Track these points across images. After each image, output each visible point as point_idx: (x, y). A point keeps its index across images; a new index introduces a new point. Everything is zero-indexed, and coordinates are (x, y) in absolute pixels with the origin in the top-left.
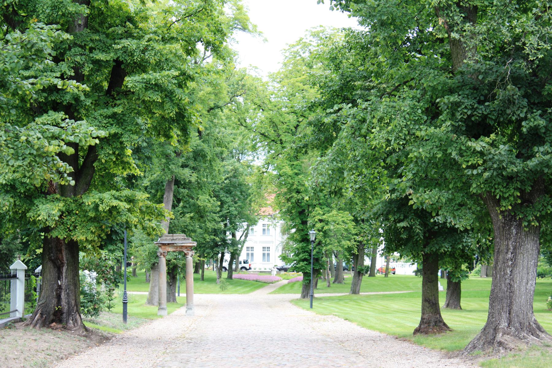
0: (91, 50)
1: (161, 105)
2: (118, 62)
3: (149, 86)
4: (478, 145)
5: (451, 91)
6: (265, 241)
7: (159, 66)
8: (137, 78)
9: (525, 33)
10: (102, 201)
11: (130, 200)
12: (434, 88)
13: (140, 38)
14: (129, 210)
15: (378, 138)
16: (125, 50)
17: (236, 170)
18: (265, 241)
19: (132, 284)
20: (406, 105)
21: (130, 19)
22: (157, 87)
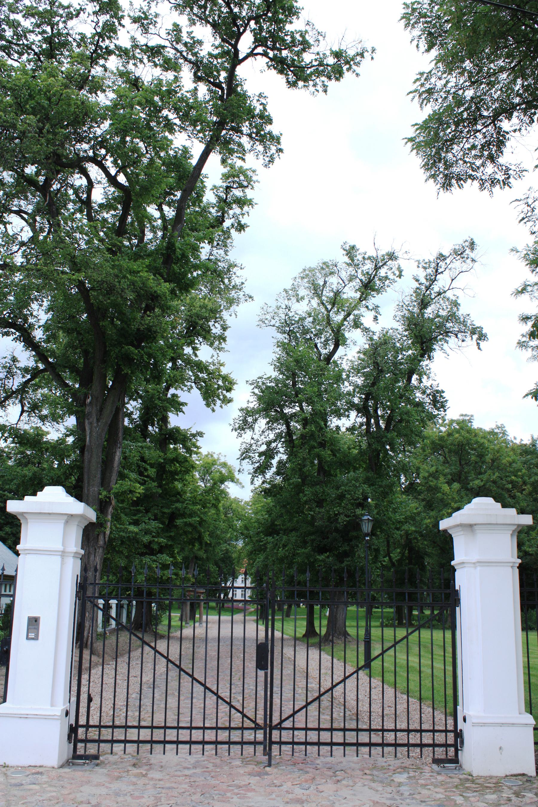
0: (162, 507)
1: (191, 533)
2: (173, 513)
3: (186, 524)
4: (321, 557)
5: (312, 534)
6: (241, 587)
7: (191, 516)
8: (181, 521)
9: (339, 514)
10: (164, 575)
11: (176, 574)
12: (305, 532)
13: (183, 502)
14: (176, 579)
15: (281, 552)
16: (176, 508)
17: (227, 550)
18: (241, 587)
19: (491, 777)
20: (293, 539)
21: (179, 493)
22: (190, 525)
